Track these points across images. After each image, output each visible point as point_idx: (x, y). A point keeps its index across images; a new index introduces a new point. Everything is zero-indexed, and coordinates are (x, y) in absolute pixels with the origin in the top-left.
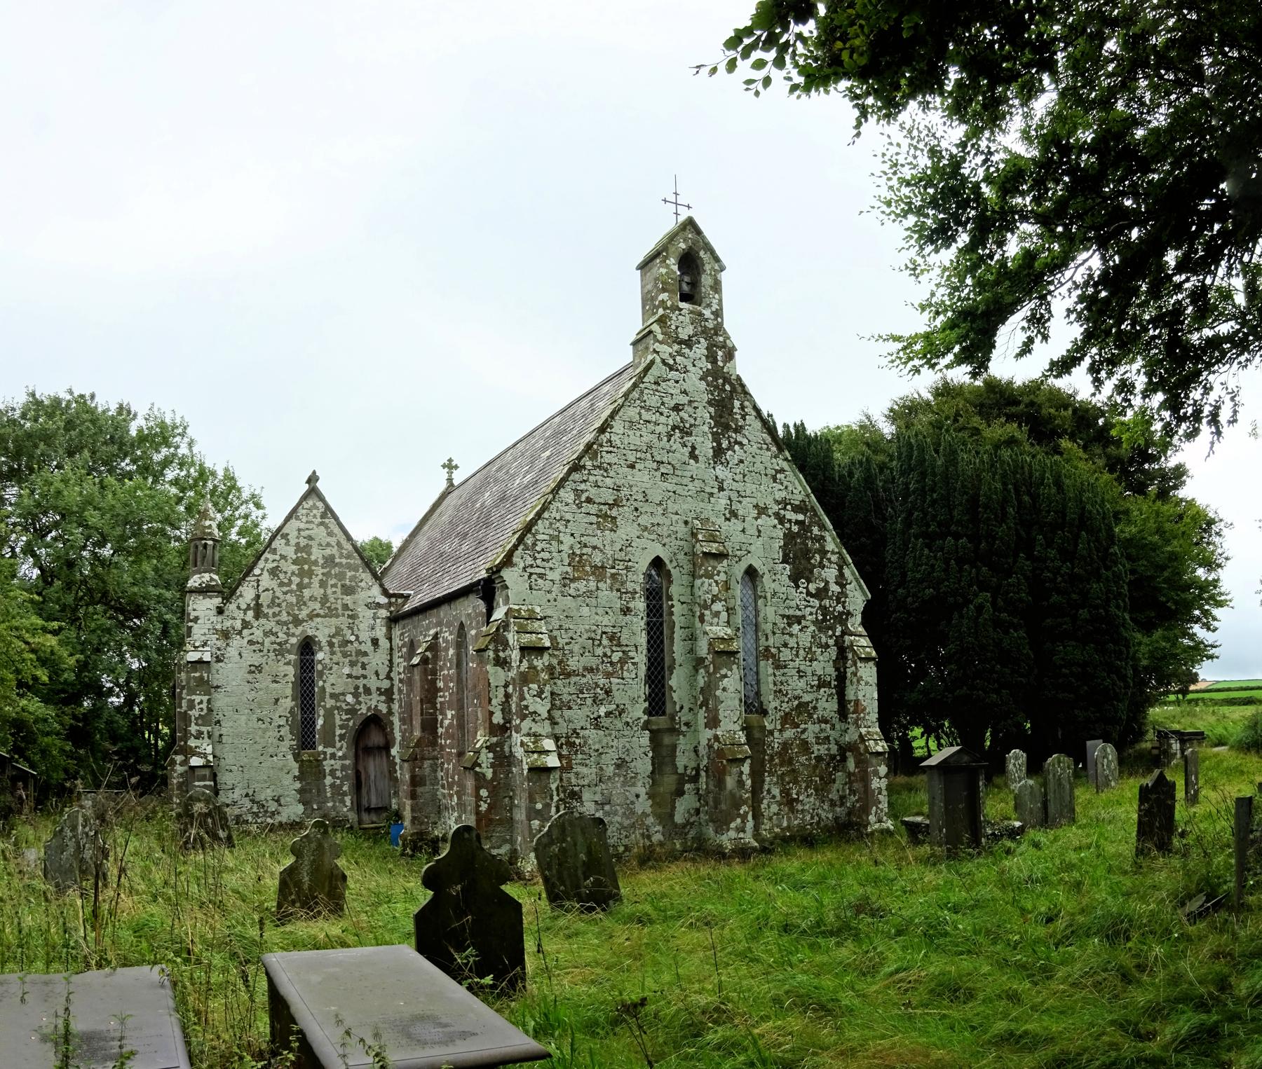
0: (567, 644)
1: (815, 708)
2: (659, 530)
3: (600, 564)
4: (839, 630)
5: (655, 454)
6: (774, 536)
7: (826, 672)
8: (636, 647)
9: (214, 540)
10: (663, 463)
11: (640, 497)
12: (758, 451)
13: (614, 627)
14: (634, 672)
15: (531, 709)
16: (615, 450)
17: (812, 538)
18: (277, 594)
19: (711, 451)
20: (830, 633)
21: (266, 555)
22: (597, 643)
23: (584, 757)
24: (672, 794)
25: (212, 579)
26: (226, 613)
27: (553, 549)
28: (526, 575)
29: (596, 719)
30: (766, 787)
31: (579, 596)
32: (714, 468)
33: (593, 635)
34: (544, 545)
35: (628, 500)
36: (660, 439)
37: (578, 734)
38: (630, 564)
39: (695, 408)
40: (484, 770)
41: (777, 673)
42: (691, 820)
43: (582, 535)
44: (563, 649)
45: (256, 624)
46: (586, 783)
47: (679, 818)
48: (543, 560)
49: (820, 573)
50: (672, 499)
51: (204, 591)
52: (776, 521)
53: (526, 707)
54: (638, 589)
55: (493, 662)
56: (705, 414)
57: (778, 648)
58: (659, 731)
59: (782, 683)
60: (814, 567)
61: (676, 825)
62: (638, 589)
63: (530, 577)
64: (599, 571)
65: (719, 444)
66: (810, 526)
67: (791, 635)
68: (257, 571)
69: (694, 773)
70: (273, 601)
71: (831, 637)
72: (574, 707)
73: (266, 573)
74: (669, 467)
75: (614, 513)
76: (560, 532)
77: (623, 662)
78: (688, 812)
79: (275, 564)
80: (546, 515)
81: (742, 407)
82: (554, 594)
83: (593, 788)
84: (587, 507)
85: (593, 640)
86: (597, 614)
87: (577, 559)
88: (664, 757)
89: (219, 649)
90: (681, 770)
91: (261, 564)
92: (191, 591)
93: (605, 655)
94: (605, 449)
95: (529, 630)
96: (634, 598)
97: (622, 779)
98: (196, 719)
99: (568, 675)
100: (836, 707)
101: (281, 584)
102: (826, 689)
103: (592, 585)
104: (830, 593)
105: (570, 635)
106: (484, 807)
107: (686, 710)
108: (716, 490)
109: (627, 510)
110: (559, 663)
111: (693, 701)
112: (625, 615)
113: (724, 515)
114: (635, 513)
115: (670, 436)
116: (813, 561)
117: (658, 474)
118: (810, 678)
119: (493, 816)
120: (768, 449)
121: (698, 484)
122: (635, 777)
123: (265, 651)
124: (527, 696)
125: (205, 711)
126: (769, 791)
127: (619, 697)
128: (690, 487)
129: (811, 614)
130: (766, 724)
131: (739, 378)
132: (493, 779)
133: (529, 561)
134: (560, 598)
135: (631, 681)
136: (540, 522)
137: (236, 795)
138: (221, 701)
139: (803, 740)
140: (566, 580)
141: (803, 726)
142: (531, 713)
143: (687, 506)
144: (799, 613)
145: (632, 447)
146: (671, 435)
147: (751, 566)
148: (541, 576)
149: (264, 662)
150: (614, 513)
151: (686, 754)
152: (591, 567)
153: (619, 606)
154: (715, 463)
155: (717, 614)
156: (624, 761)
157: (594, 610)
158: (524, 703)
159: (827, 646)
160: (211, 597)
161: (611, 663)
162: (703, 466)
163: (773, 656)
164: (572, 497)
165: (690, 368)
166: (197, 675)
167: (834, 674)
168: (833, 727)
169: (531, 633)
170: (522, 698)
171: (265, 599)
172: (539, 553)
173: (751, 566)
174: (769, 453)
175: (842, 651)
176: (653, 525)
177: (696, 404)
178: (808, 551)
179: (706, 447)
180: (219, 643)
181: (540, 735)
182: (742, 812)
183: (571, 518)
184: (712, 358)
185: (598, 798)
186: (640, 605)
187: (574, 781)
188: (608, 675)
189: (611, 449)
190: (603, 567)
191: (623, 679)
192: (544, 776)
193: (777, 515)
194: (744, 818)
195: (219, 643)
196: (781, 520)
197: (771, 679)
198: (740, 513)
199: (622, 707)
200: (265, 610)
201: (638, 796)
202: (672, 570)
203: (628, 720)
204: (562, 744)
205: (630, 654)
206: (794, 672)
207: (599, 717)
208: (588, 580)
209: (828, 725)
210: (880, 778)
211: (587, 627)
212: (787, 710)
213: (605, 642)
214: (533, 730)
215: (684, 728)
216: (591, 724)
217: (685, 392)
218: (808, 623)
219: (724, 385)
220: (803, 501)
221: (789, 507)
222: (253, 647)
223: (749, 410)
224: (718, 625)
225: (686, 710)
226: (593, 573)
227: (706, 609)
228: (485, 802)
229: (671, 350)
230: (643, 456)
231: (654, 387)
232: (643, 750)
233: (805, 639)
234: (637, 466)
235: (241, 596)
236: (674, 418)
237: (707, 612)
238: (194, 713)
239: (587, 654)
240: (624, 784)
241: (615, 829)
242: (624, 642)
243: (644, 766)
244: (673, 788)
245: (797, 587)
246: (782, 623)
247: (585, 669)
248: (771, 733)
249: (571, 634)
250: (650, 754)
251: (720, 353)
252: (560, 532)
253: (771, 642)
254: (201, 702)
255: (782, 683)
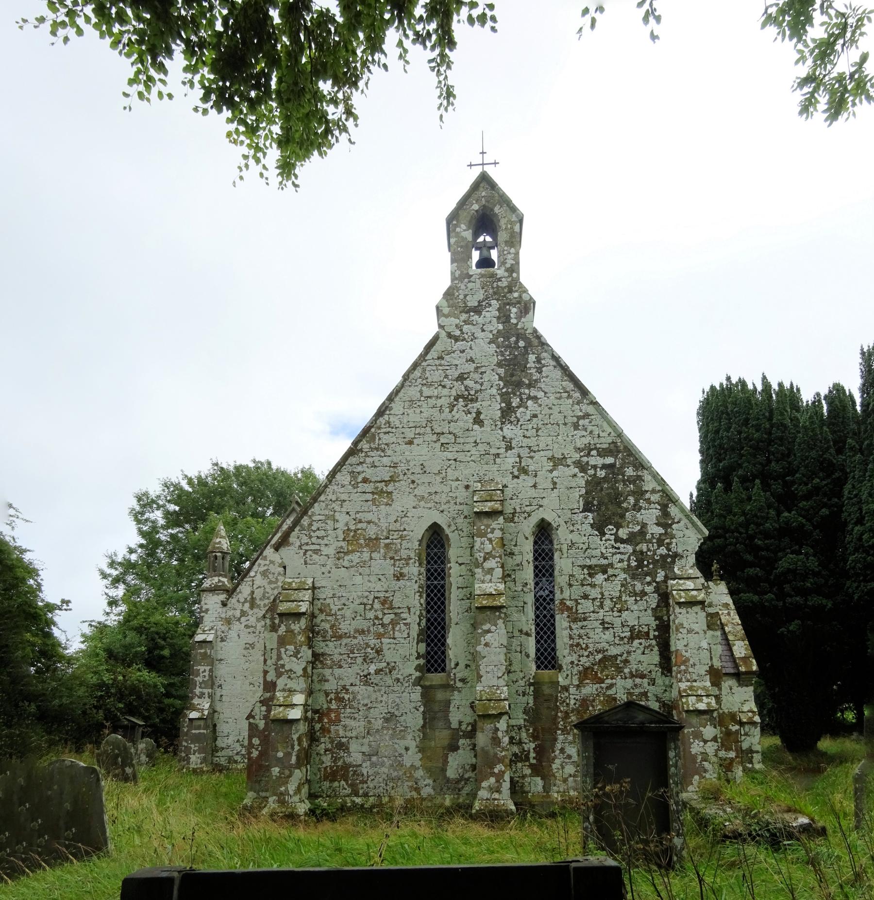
0: (339, 610)
1: (626, 661)
2: (437, 498)
3: (374, 537)
4: (660, 576)
5: (435, 427)
6: (574, 485)
7: (642, 621)
8: (409, 609)
9: (221, 552)
10: (443, 434)
11: (418, 470)
12: (556, 402)
13: (386, 592)
14: (406, 632)
15: (287, 668)
16: (394, 430)
17: (624, 481)
18: (267, 590)
19: (499, 412)
20: (648, 579)
21: (259, 561)
22: (368, 607)
23: (353, 711)
24: (444, 748)
25: (220, 581)
26: (229, 605)
27: (329, 528)
28: (302, 552)
29: (365, 676)
30: (559, 746)
31: (352, 567)
32: (501, 429)
33: (365, 601)
34: (320, 524)
35: (405, 474)
36: (441, 411)
37: (347, 690)
38: (405, 533)
39: (482, 373)
40: (258, 722)
41: (573, 627)
42: (466, 776)
43: (358, 512)
44: (335, 615)
45: (251, 612)
46: (354, 734)
47: (451, 773)
48: (318, 537)
49: (634, 516)
50: (453, 467)
51: (213, 590)
52: (577, 470)
53: (283, 666)
54: (412, 555)
55: (269, 628)
56: (493, 378)
57: (576, 600)
58: (431, 687)
59: (580, 636)
60: (627, 510)
61: (448, 780)
62: (412, 555)
63: (305, 554)
64: (373, 543)
65: (509, 404)
66: (622, 467)
67: (593, 586)
68: (252, 574)
69: (469, 728)
70: (264, 596)
71: (649, 584)
72: (345, 666)
73: (259, 575)
74: (451, 436)
75: (390, 488)
76: (335, 512)
77: (394, 623)
78: (463, 767)
79: (266, 568)
80: (322, 498)
81: (539, 360)
82: (328, 567)
83: (360, 740)
84: (362, 487)
85: (365, 605)
86: (369, 581)
87: (352, 534)
88: (436, 713)
89: (223, 632)
90: (455, 725)
91: (255, 568)
92: (203, 591)
93: (377, 618)
94: (384, 430)
95: (293, 598)
96: (407, 564)
97: (390, 732)
98: (200, 683)
99: (340, 637)
100: (656, 659)
101: (270, 582)
102: (643, 641)
103: (366, 556)
104: (648, 537)
105: (343, 602)
106: (255, 754)
107: (462, 666)
108: (502, 451)
109: (403, 485)
110: (332, 627)
111: (470, 657)
112: (398, 579)
113: (512, 473)
114: (412, 486)
115: (452, 407)
116: (625, 505)
117: (438, 445)
118: (618, 630)
119: (263, 762)
120: (569, 397)
121: (481, 447)
122: (404, 731)
123: (257, 632)
124: (284, 656)
125: (207, 678)
126: (562, 750)
127: (389, 655)
128: (472, 452)
129: (621, 561)
130: (560, 679)
131: (535, 331)
132: (264, 730)
133: (305, 539)
134: (334, 570)
135: (402, 641)
136: (316, 505)
137: (230, 741)
138: (222, 670)
139: (609, 696)
140: (340, 554)
141: (609, 681)
142: (287, 671)
143: (468, 472)
144: (605, 562)
145: (411, 425)
146: (454, 406)
147: (543, 520)
148: (316, 552)
149: (256, 640)
150: (390, 488)
151: (462, 709)
152: (365, 540)
153: (392, 572)
154: (503, 423)
155: (490, 571)
156: (393, 715)
157: (367, 578)
158: (281, 662)
159: (643, 594)
160: (218, 594)
161: (383, 625)
162: (489, 429)
163: (569, 609)
164: (349, 479)
165: (479, 334)
166: (202, 651)
167: (654, 624)
168: (653, 682)
169: (293, 601)
170: (279, 658)
171: (258, 594)
172: (314, 531)
173: (543, 520)
174: (570, 401)
175: (664, 597)
176: (430, 494)
177: (483, 369)
178: (618, 494)
179: (492, 408)
180: (223, 628)
181: (295, 691)
182: (496, 771)
183: (346, 498)
184: (504, 317)
185: (365, 749)
186: (414, 570)
187: (341, 733)
188: (379, 636)
189: (390, 429)
190: (377, 539)
191: (394, 638)
192: (286, 728)
193: (578, 464)
194: (499, 777)
195: (223, 628)
196: (583, 468)
197: (566, 633)
198: (531, 468)
199: (393, 664)
200: (258, 602)
201: (407, 749)
202: (450, 535)
203: (399, 676)
204: (331, 699)
205: (402, 615)
206: (597, 624)
207: (369, 674)
208: (362, 552)
209: (646, 681)
210: (705, 742)
211: (360, 594)
212: (587, 665)
213: (377, 605)
214: (288, 686)
215: (459, 684)
216: (361, 681)
217: (472, 360)
218: (616, 572)
219: (517, 342)
220: (613, 442)
221: (594, 453)
222: (249, 630)
223: (547, 360)
224: (491, 581)
225: (462, 666)
226: (367, 545)
227: (477, 567)
228: (257, 749)
229: (457, 321)
230: (422, 431)
231: (437, 362)
232: (413, 705)
233: (613, 589)
234: (415, 441)
235: (240, 592)
236: (459, 388)
237: (478, 571)
238: (199, 679)
239: (358, 617)
240: (392, 737)
241: (381, 780)
242: (395, 605)
243: (415, 720)
244: (446, 742)
245: (603, 534)
246: (580, 574)
247: (357, 631)
248: (566, 689)
249: (343, 600)
250: (422, 709)
251: (514, 310)
252: (335, 512)
253: (566, 595)
254: (205, 671)
255: (580, 636)
